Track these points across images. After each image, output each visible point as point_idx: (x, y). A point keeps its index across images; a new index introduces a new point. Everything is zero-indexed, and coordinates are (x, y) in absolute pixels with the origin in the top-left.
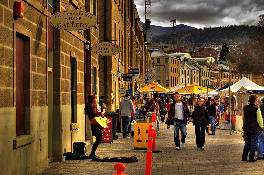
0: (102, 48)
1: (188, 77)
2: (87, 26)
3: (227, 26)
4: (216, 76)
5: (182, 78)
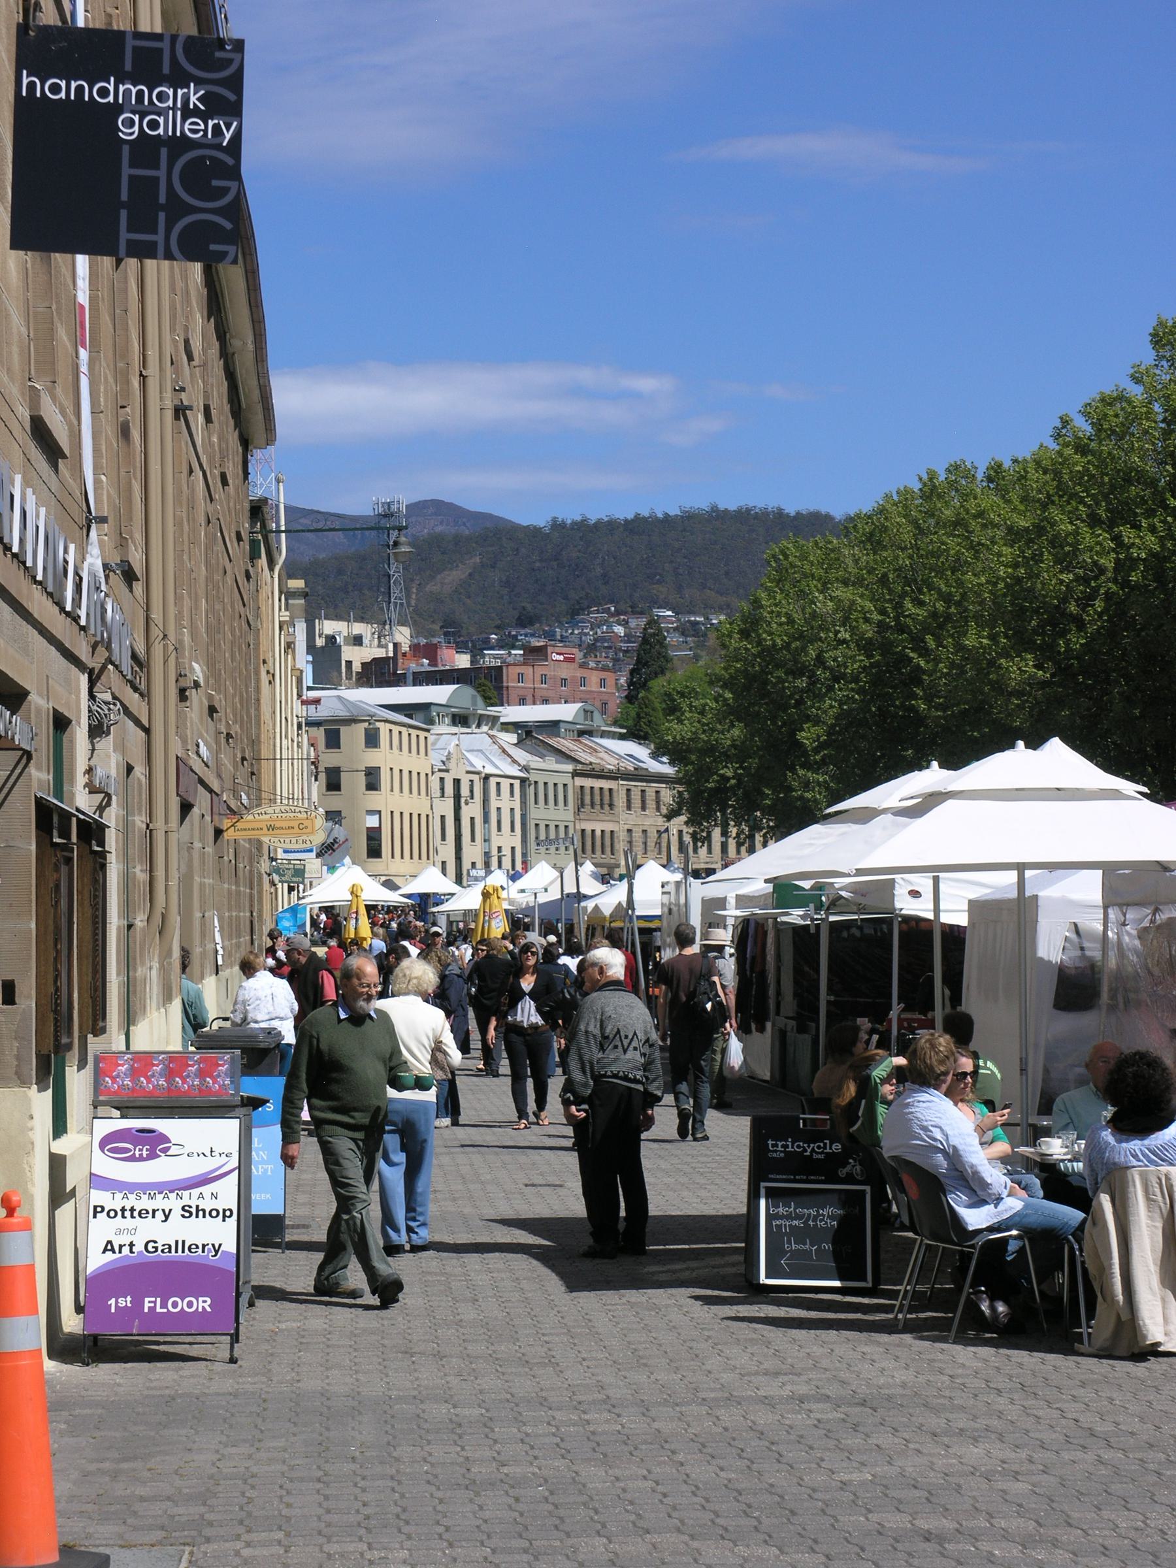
4: (606, 802)
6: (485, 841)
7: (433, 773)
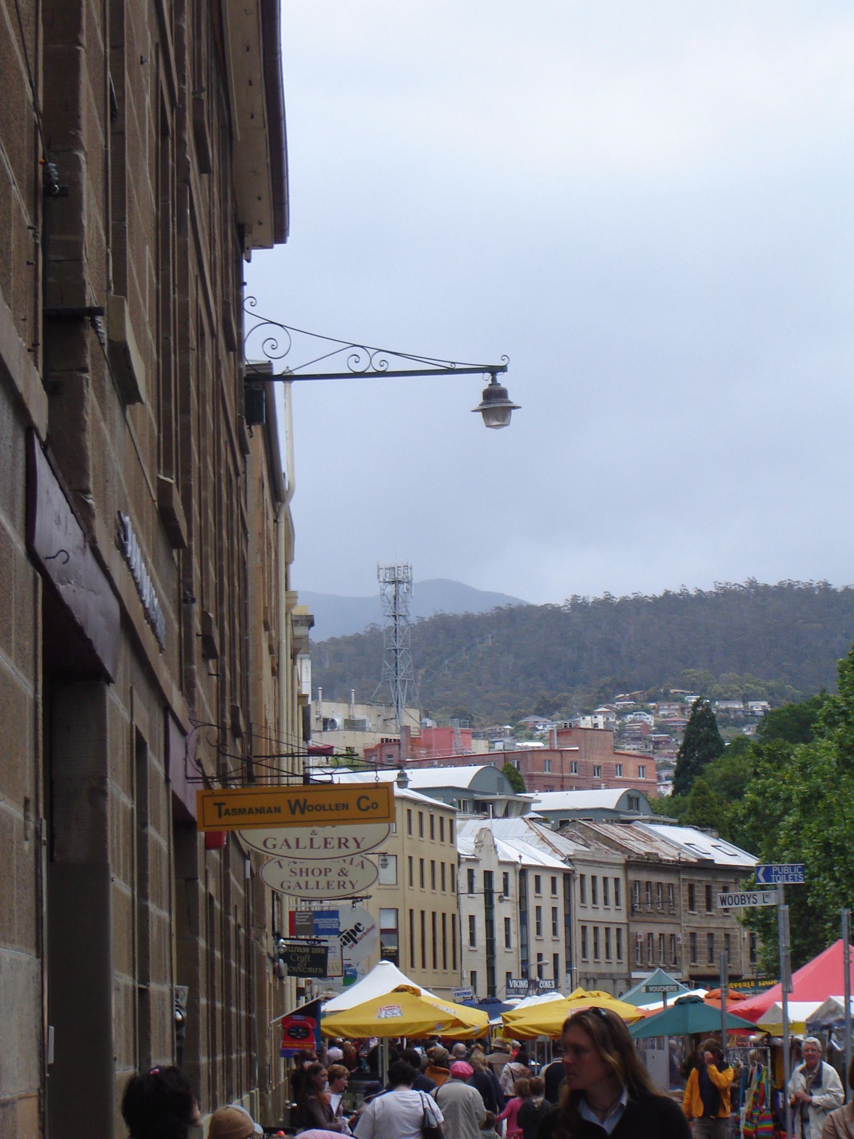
0: (304, 870)
1: (505, 910)
2: (358, 847)
3: (708, 587)
5: (472, 918)
6: (522, 946)
7: (459, 863)
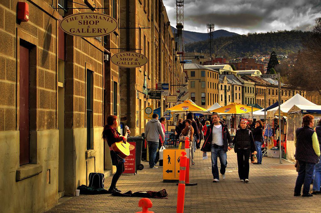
0: (124, 59)
1: (229, 94)
2: (105, 32)
3: (276, 31)
4: (263, 93)
5: (222, 95)
